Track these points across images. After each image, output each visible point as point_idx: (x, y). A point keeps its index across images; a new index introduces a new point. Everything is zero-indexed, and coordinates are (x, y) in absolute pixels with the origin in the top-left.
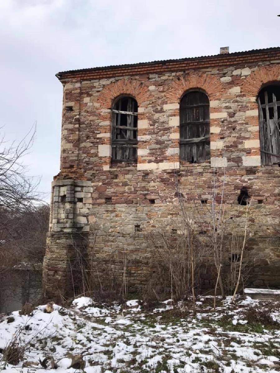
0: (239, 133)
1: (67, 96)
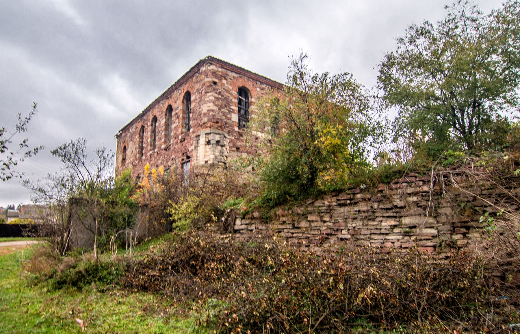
1: (43, 259)
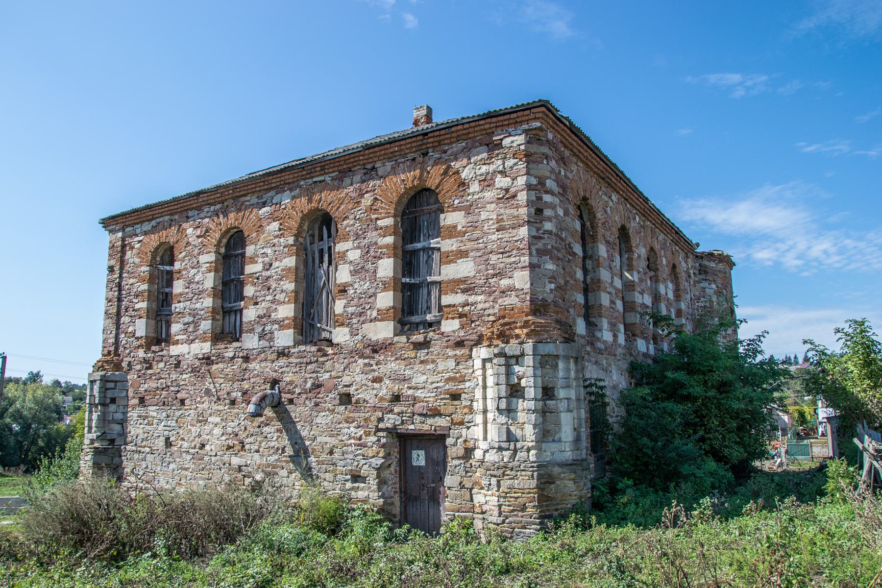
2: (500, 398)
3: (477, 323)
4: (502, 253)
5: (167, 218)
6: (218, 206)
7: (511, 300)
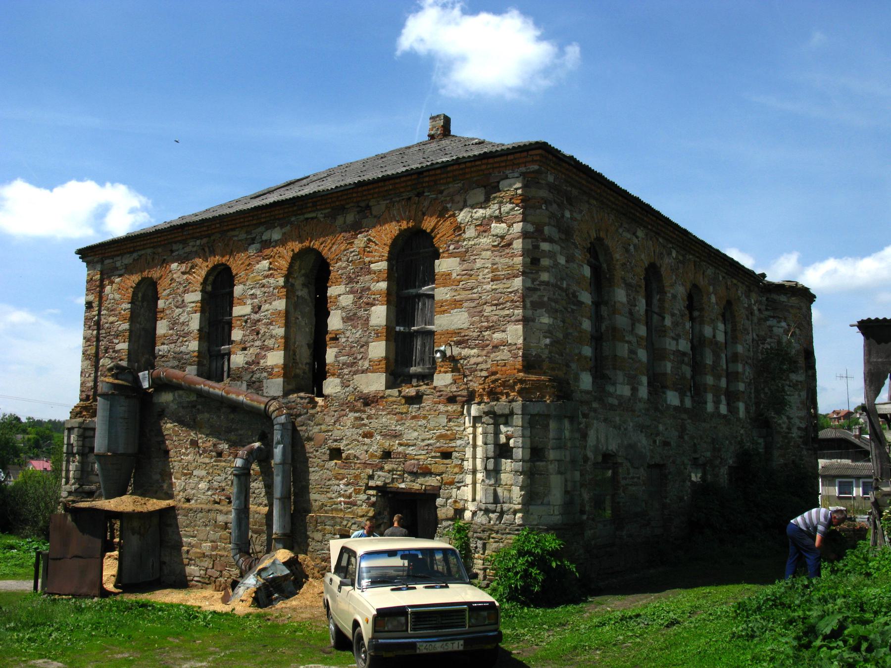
0: (263, 339)
2: (488, 458)
3: (470, 378)
4: (496, 305)
5: (149, 251)
6: (205, 240)
7: (503, 355)
